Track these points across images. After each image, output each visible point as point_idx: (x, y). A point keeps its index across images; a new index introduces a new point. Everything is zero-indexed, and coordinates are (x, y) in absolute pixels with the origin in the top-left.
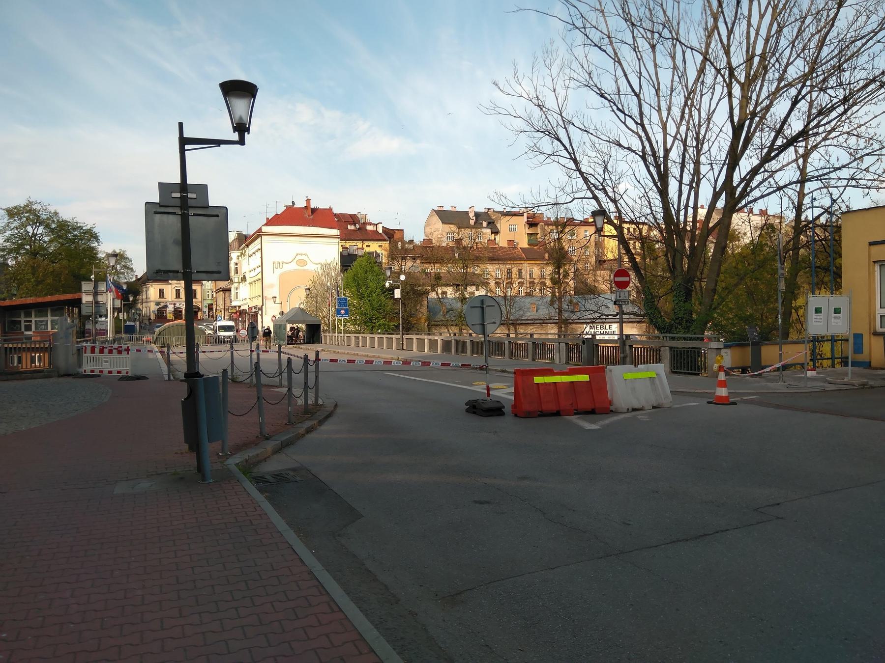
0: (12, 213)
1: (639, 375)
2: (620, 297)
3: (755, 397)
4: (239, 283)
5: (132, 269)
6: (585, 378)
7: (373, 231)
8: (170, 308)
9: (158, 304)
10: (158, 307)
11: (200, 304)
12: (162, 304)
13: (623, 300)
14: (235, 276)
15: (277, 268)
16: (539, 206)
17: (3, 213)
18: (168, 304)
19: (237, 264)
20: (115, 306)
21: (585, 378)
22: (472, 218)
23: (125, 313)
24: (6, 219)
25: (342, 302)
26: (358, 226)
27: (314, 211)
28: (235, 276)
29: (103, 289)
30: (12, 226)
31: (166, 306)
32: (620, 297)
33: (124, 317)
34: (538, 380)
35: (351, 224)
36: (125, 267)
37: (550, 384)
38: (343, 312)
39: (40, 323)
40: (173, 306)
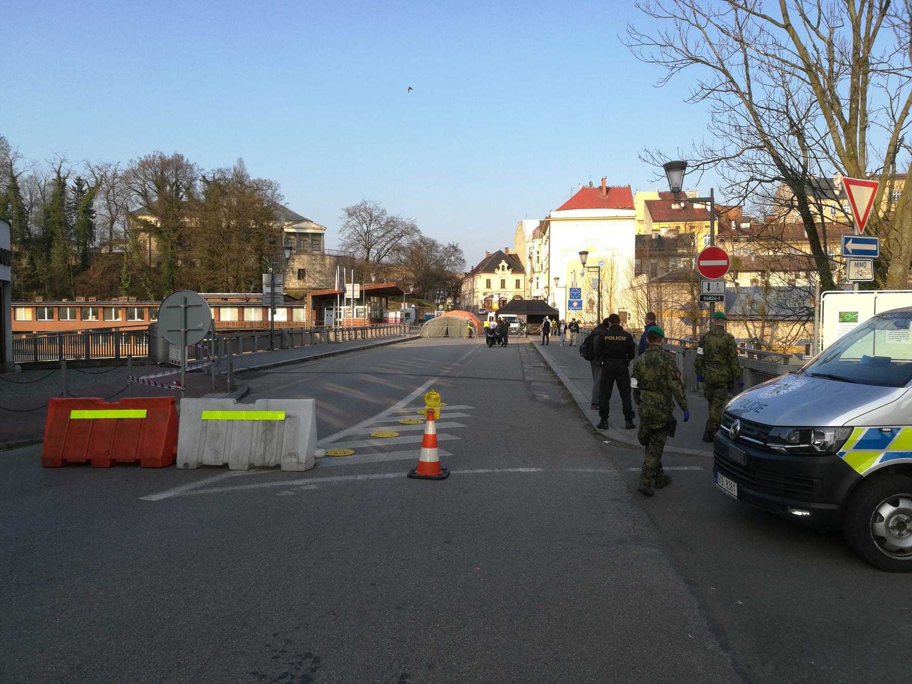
0: (351, 213)
1: (244, 415)
2: (709, 290)
3: (533, 470)
4: (540, 272)
5: (464, 261)
6: (141, 414)
7: (702, 209)
8: (496, 299)
9: (485, 294)
10: (485, 297)
11: (523, 294)
12: (489, 294)
13: (714, 295)
14: (537, 266)
15: (564, 256)
16: (703, 163)
17: (344, 212)
18: (494, 294)
19: (538, 253)
20: (355, 297)
21: (141, 414)
22: (837, 186)
23: (406, 304)
24: (347, 219)
25: (575, 293)
26: (683, 205)
27: (608, 189)
28: (537, 266)
29: (280, 281)
30: (350, 224)
31: (492, 296)
32: (709, 290)
33: (405, 307)
34: (76, 414)
35: (675, 203)
36: (457, 258)
37: (88, 420)
38: (575, 304)
39: (348, 311)
40: (498, 295)
